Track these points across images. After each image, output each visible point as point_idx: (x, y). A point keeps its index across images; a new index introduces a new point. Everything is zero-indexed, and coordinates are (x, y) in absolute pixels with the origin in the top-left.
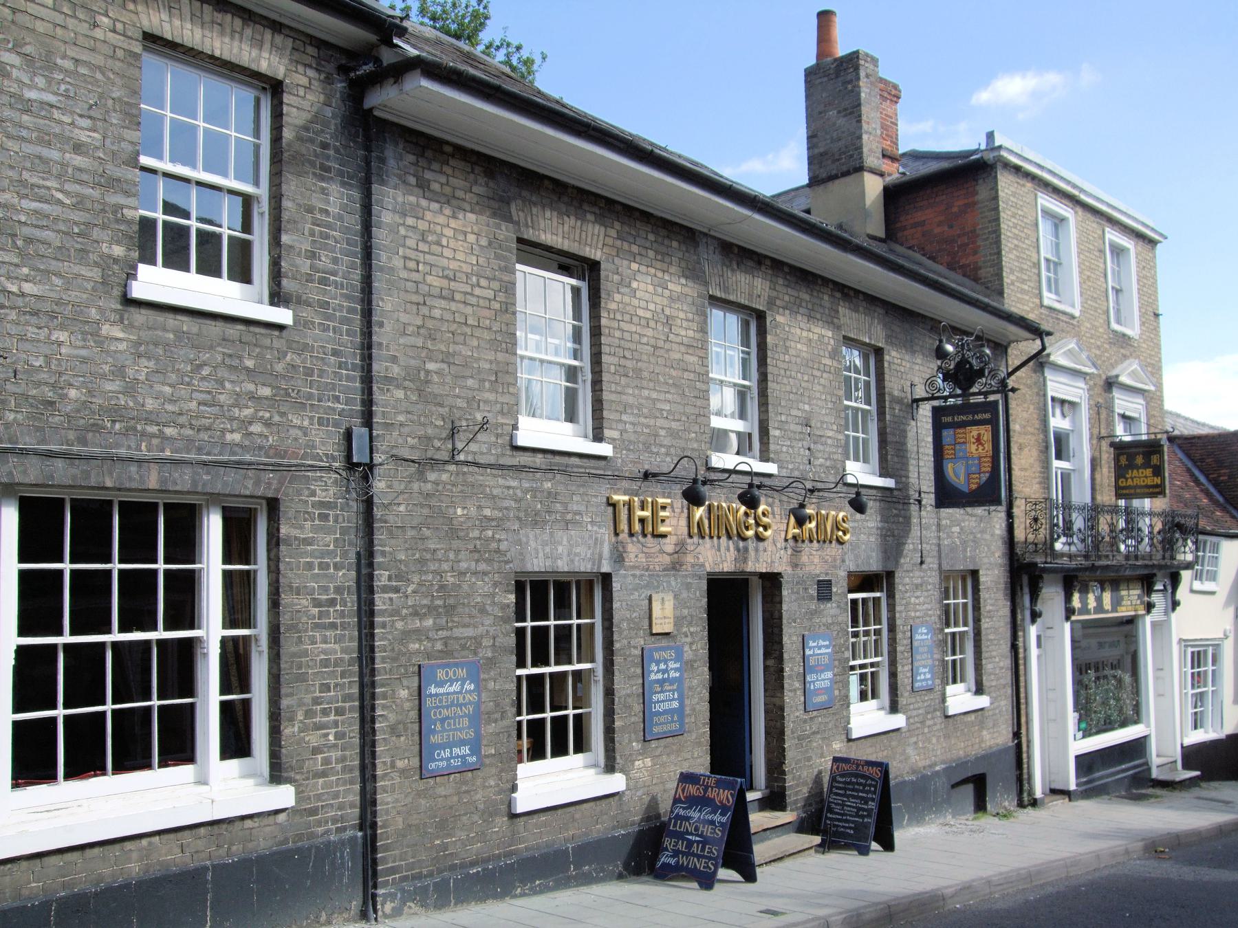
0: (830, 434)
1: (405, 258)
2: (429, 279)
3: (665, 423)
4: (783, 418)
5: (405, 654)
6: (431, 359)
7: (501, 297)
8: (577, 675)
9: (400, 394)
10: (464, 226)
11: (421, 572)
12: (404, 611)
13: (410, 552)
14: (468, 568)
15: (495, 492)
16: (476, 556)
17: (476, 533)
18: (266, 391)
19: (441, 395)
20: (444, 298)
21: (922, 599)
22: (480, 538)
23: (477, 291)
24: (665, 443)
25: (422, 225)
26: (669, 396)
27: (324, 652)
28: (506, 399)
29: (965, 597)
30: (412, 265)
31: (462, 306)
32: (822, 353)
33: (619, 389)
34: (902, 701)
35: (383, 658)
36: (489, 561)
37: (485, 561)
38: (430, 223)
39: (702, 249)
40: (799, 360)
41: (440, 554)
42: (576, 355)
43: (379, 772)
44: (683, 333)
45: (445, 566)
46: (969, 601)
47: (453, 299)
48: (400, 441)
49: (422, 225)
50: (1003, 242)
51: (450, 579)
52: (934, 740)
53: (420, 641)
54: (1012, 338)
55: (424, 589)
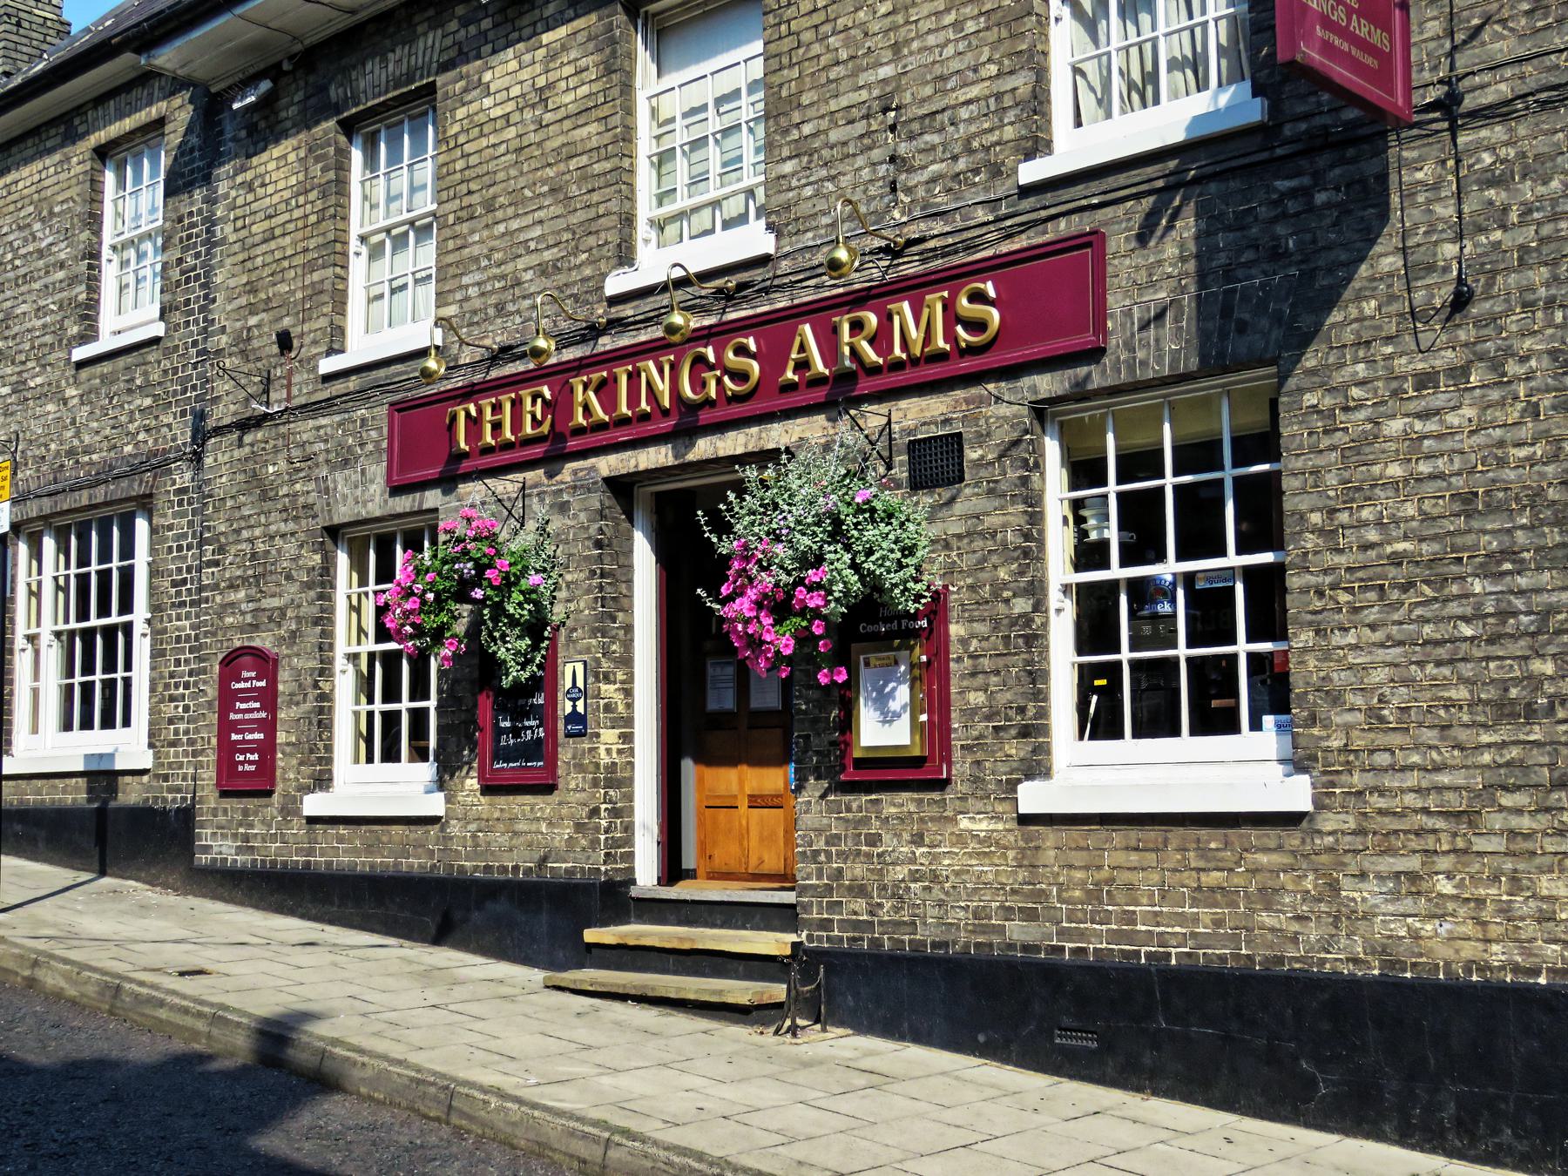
16: (284, 515)
18: (148, 402)
27: (178, 629)
36: (296, 518)
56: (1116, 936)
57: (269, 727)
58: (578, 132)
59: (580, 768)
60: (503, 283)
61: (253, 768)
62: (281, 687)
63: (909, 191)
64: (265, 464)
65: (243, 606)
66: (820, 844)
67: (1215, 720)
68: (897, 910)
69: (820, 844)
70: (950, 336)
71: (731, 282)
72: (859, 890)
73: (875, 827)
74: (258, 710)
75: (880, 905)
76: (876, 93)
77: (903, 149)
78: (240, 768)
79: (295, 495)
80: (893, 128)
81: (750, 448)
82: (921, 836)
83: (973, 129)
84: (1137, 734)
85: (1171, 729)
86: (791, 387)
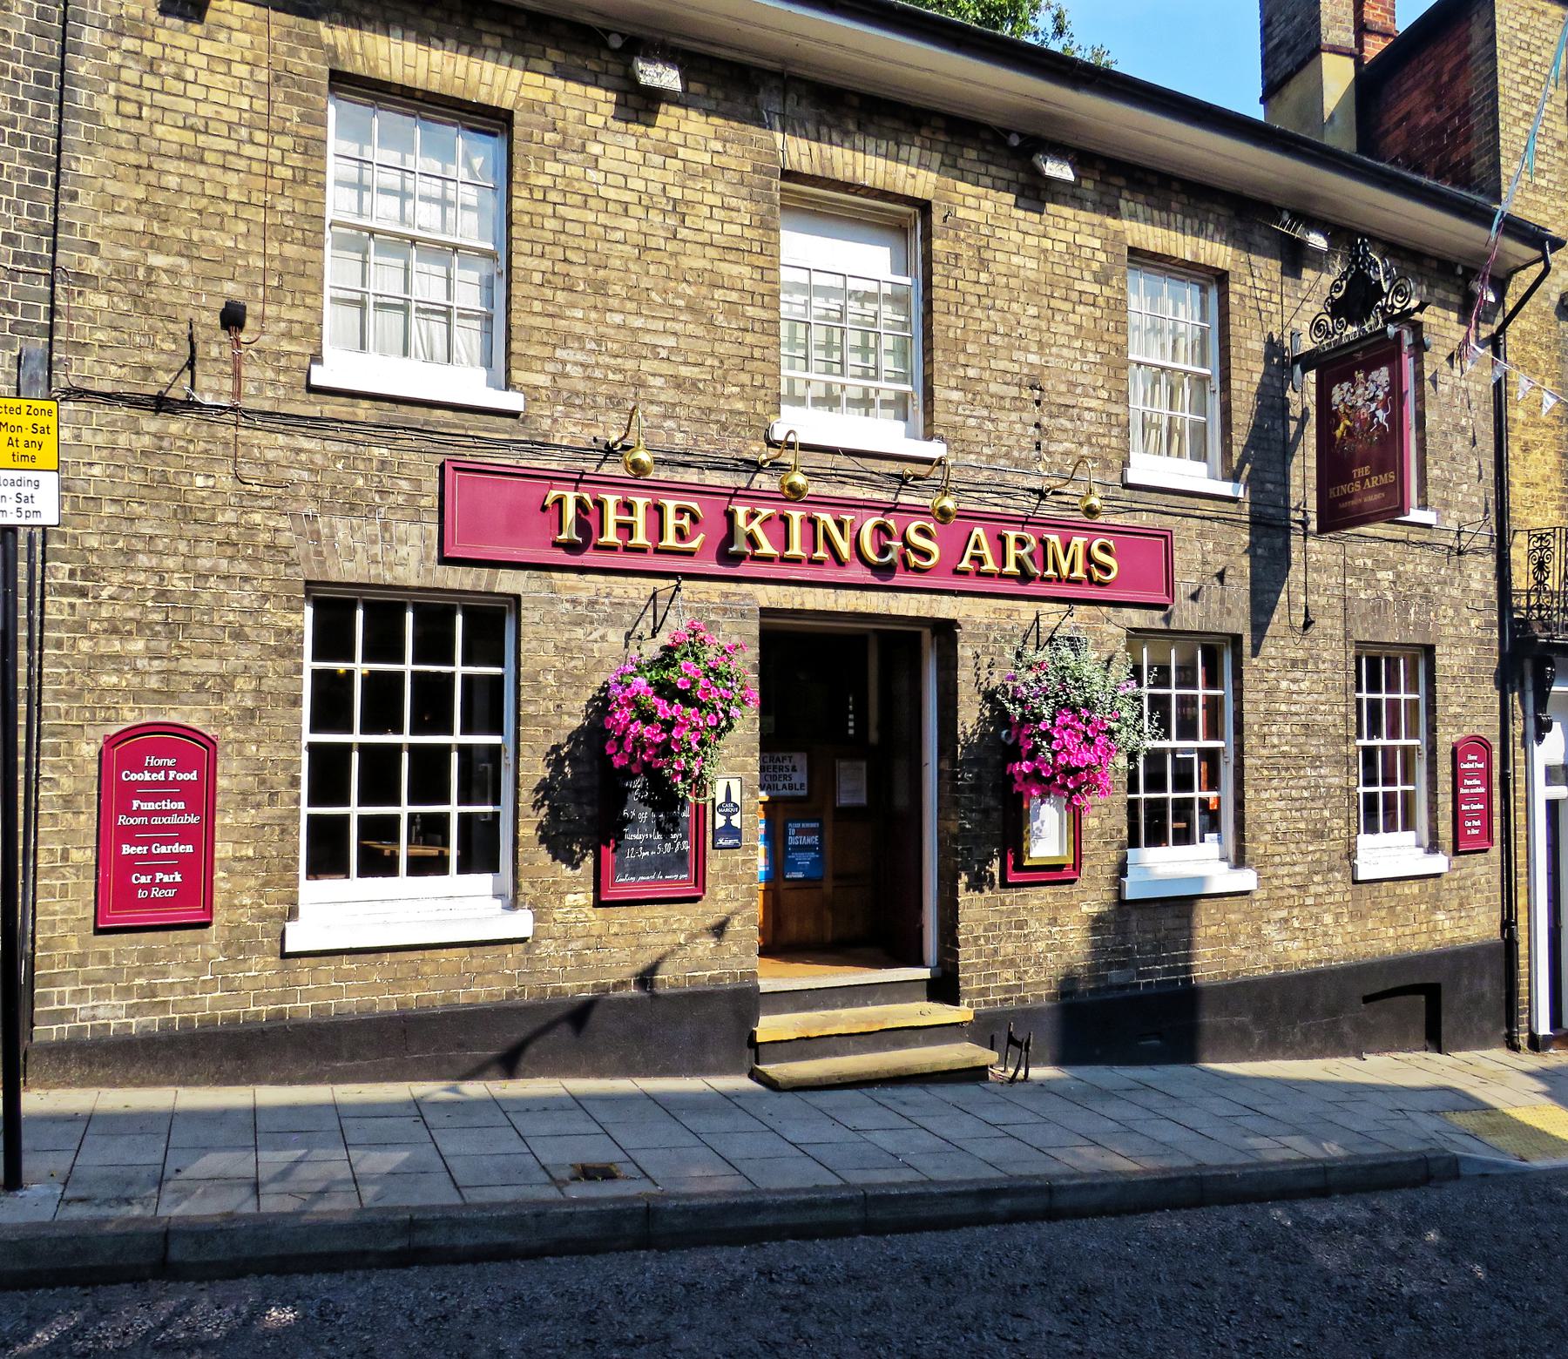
0: (1093, 403)
1: (118, 98)
2: (159, 130)
3: (666, 369)
4: (971, 373)
5: (92, 690)
6: (158, 250)
7: (296, 160)
8: (1405, 749)
9: (101, 300)
10: (229, 51)
11: (125, 569)
12: (94, 625)
13: (108, 538)
14: (211, 569)
15: (270, 455)
16: (229, 551)
17: (230, 516)
19: (174, 305)
20: (186, 159)
21: (1304, 686)
22: (236, 525)
23: (248, 150)
24: (663, 398)
25: (150, 50)
26: (678, 327)
28: (298, 314)
29: (1412, 687)
30: (130, 108)
31: (218, 172)
32: (1075, 273)
33: (550, 309)
34: (1254, 849)
35: (56, 693)
36: (254, 560)
37: (244, 559)
38: (164, 45)
39: (762, 96)
40: (1013, 282)
41: (160, 545)
42: (1203, 319)
43: (42, 864)
44: (716, 227)
45: (170, 563)
46: (1420, 696)
47: (202, 162)
48: (97, 370)
49: (150, 50)
50: (1502, 107)
51: (178, 584)
52: (1328, 919)
53: (119, 671)
54: (1513, 262)
55: (129, 594)
56: (1168, 972)
57: (203, 836)
58: (722, 264)
59: (732, 879)
60: (619, 377)
61: (171, 893)
62: (222, 782)
63: (1049, 453)
64: (190, 471)
65: (140, 664)
66: (980, 932)
67: (1184, 837)
68: (1037, 973)
69: (980, 932)
70: (1088, 572)
71: (909, 468)
72: (1011, 963)
73: (1023, 915)
74: (180, 813)
75: (1026, 972)
76: (1025, 371)
77: (1045, 421)
78: (141, 894)
79: (253, 527)
80: (1038, 403)
81: (922, 614)
82: (1055, 919)
83: (1092, 429)
84: (363, 873)
85: (341, 869)
86: (965, 573)
